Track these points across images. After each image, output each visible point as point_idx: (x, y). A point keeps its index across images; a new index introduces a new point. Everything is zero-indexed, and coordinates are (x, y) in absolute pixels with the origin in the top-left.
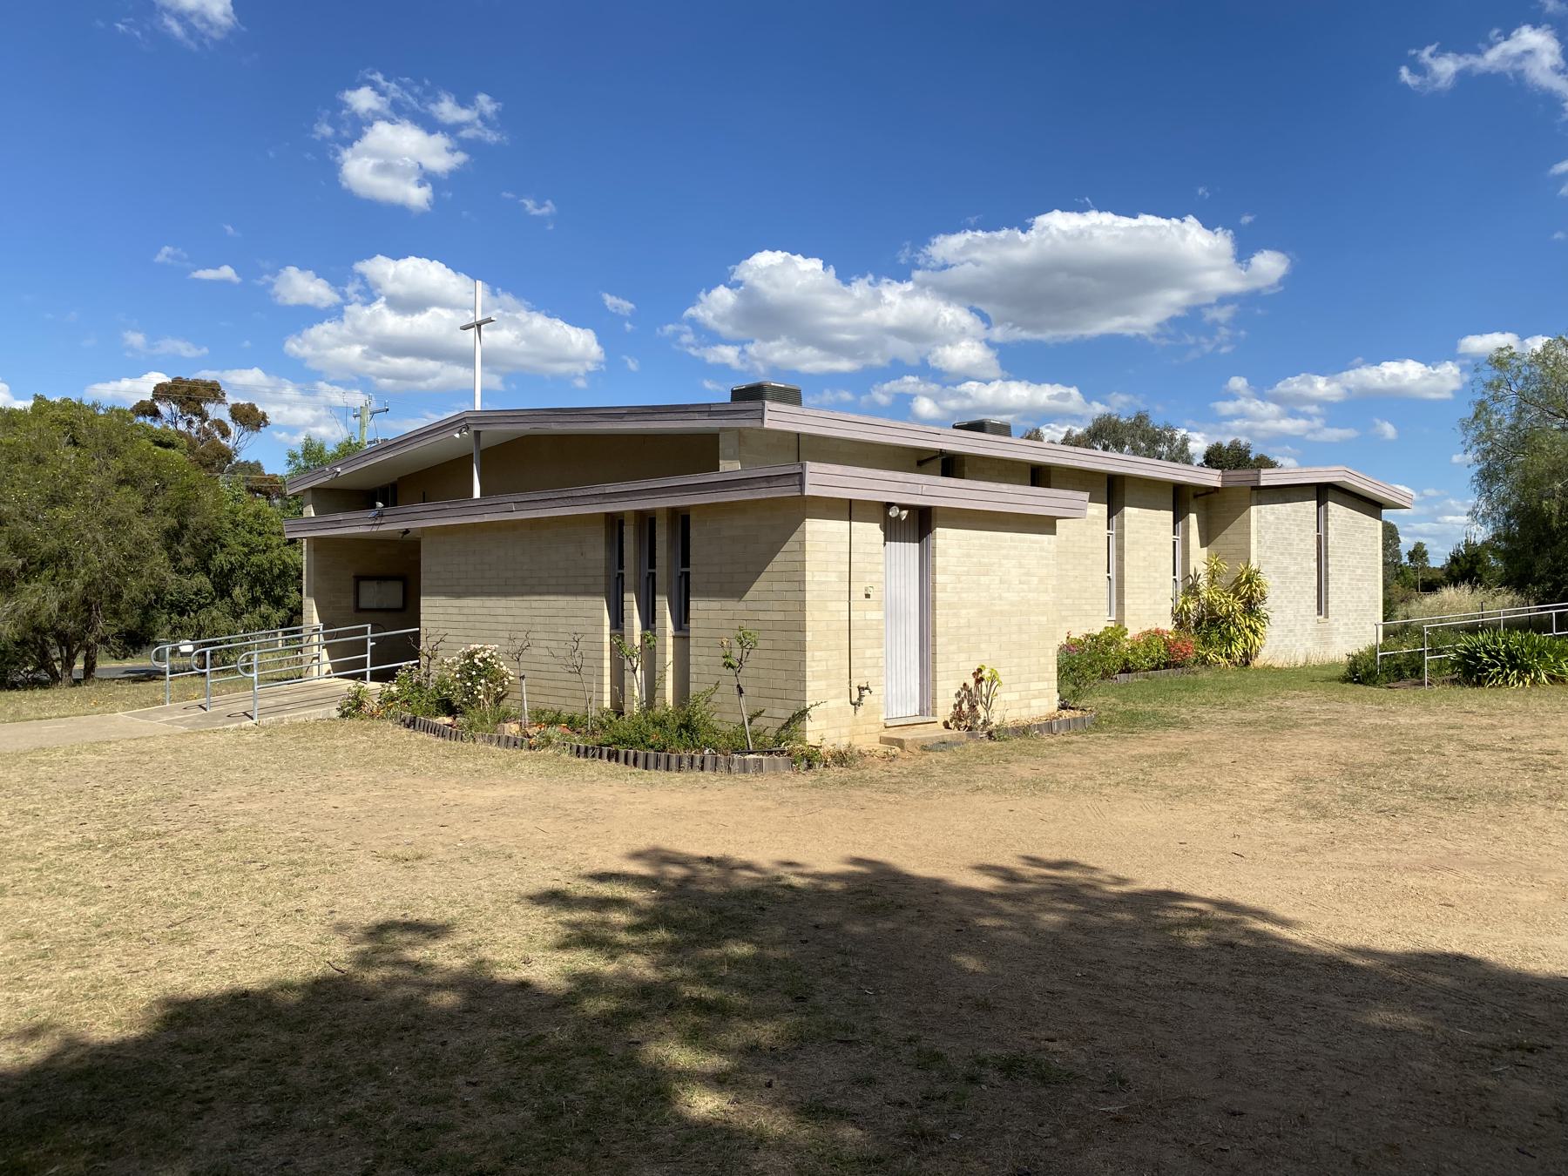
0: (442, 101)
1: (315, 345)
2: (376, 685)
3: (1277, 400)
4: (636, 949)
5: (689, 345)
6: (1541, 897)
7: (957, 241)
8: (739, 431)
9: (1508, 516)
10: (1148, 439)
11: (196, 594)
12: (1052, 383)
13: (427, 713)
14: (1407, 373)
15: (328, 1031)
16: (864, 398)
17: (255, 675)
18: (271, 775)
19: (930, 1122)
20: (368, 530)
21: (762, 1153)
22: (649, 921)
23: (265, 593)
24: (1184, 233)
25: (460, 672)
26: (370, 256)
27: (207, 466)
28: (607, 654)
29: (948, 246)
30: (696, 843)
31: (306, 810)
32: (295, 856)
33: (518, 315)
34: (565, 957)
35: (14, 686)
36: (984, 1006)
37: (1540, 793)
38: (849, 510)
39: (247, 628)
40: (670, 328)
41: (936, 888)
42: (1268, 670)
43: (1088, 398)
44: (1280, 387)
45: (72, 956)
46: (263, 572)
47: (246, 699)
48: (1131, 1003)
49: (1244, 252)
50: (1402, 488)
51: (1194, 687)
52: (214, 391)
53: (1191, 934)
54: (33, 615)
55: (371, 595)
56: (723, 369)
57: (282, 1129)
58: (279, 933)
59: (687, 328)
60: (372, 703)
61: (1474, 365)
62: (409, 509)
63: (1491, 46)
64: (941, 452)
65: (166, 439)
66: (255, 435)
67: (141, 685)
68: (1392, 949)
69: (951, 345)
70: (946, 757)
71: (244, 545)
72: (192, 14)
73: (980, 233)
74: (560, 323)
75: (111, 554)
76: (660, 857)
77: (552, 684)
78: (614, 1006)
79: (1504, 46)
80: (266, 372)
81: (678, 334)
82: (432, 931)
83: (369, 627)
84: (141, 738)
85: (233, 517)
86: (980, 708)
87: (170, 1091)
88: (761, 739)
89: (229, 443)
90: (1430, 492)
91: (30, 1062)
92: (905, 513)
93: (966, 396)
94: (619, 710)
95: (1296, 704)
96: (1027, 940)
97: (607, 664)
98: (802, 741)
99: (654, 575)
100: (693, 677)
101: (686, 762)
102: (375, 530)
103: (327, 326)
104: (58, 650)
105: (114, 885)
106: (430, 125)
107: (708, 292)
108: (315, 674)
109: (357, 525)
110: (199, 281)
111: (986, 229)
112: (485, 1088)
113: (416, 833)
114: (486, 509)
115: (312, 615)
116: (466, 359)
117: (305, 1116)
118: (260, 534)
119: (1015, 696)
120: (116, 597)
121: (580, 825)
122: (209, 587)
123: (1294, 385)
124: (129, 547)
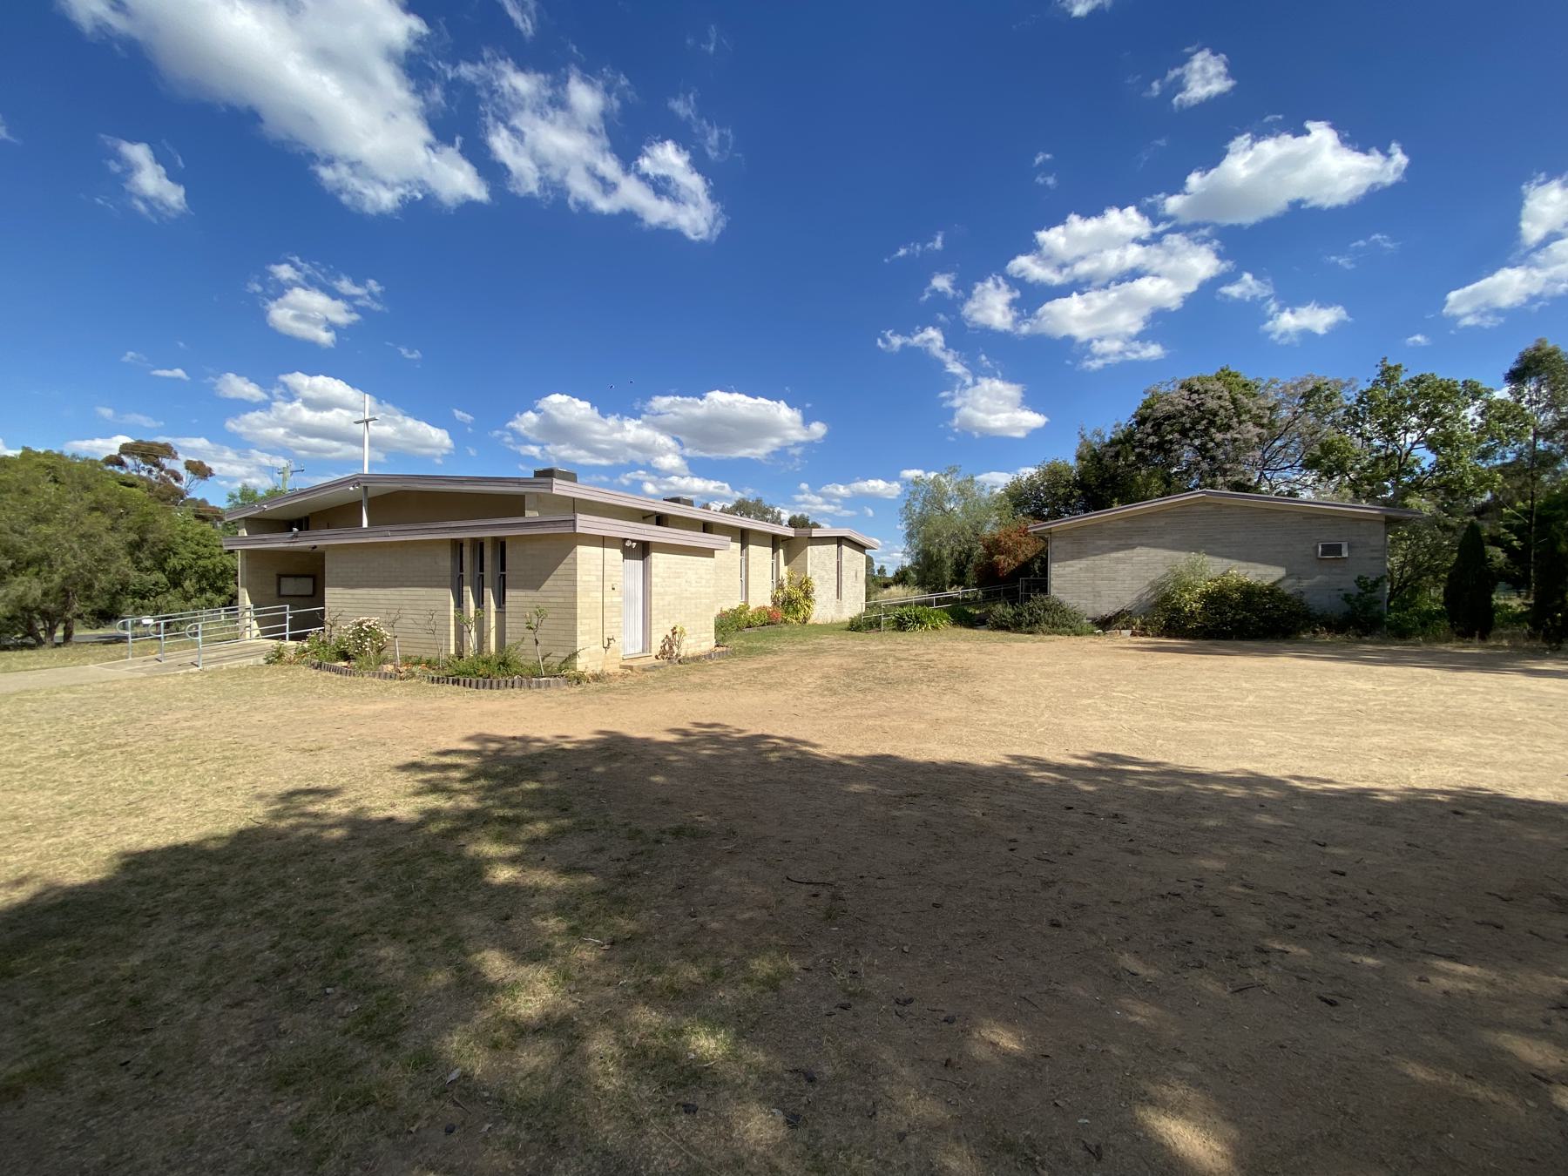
0: (342, 280)
1: (249, 425)
2: (294, 643)
3: (822, 495)
4: (465, 792)
5: (510, 443)
6: (923, 726)
7: (666, 400)
8: (538, 494)
9: (918, 554)
10: (762, 512)
11: (154, 585)
12: (716, 480)
13: (330, 660)
14: (878, 485)
15: (247, 862)
16: (616, 481)
17: (199, 638)
18: (212, 703)
19: (633, 867)
20: (287, 545)
21: (537, 898)
22: (475, 775)
23: (210, 585)
24: (779, 409)
25: (353, 634)
26: (292, 372)
27: (164, 500)
28: (452, 622)
29: (661, 402)
30: (506, 728)
31: (238, 724)
32: (227, 754)
33: (397, 418)
34: (419, 801)
35: (6, 648)
36: (667, 802)
37: (925, 679)
38: (603, 541)
39: (196, 608)
40: (497, 433)
41: (646, 742)
42: (814, 625)
43: (734, 489)
44: (824, 489)
45: (50, 830)
46: (208, 571)
47: (192, 654)
48: (741, 792)
49: (807, 421)
50: (875, 540)
51: (779, 634)
52: (168, 451)
53: (771, 755)
54: (20, 599)
55: (289, 586)
56: (531, 459)
57: (211, 926)
58: (211, 804)
59: (509, 434)
60: (290, 655)
61: (907, 483)
62: (316, 532)
63: (916, 334)
64: (655, 512)
65: (129, 481)
66: (203, 482)
67: (110, 646)
68: (861, 755)
69: (662, 455)
70: (655, 674)
71: (192, 553)
72: (153, 199)
73: (678, 398)
74: (424, 424)
75: (84, 558)
76: (483, 739)
77: (417, 640)
78: (449, 826)
79: (922, 335)
80: (210, 440)
81: (502, 437)
82: (327, 793)
83: (288, 606)
84: (107, 682)
85: (183, 534)
86: (675, 648)
87: (127, 911)
88: (550, 669)
89: (181, 486)
90: (887, 542)
91: (17, 901)
92: (634, 544)
93: (672, 484)
94: (460, 657)
95: (827, 641)
96: (690, 765)
97: (452, 628)
98: (574, 669)
99: (483, 576)
100: (508, 635)
101: (502, 684)
102: (291, 545)
103: (258, 414)
104: (41, 623)
105: (84, 780)
106: (334, 295)
107: (521, 414)
108: (248, 636)
109: (279, 542)
110: (157, 377)
111: (682, 396)
112: (361, 884)
113: (320, 734)
114: (370, 534)
115: (245, 599)
116: (359, 442)
117: (229, 916)
118: (205, 546)
119: (693, 641)
120: (89, 587)
121: (432, 723)
122: (165, 580)
123: (829, 489)
124: (99, 554)
